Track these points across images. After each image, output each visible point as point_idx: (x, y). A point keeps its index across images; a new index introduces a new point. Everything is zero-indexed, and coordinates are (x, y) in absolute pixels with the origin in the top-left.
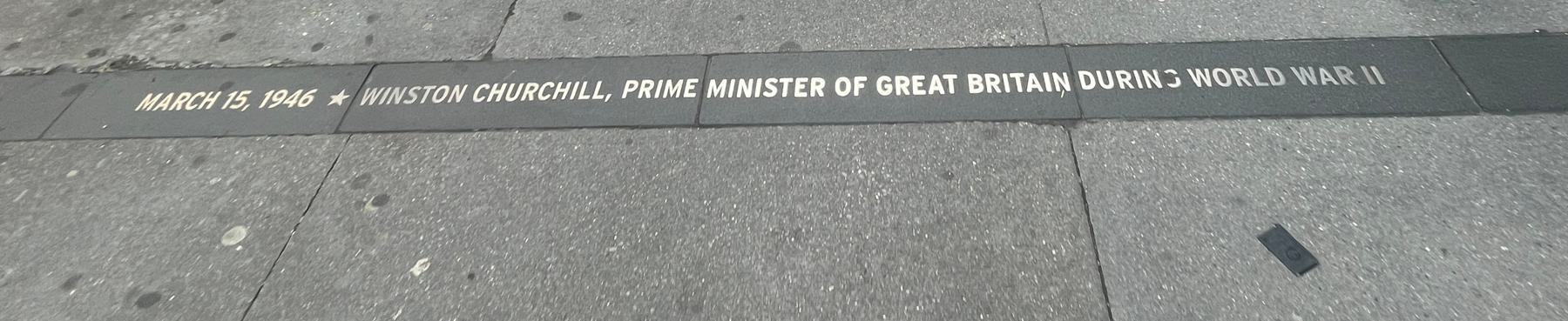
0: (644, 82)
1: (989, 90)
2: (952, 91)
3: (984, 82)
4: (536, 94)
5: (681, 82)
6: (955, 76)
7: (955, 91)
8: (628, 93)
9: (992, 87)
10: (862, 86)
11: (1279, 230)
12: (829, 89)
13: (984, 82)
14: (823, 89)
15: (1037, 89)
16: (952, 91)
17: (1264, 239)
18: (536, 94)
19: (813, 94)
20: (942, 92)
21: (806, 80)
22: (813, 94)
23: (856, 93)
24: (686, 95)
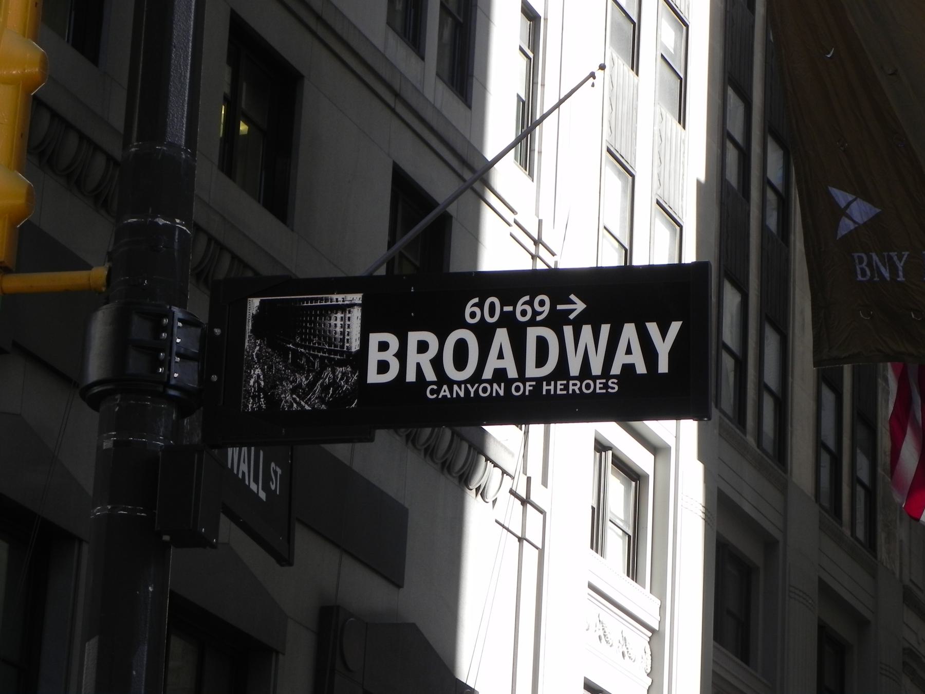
0: (414, 337)
1: (411, 377)
2: (663, 367)
3: (402, 355)
4: (437, 363)
5: (476, 385)
6: (846, 226)
7: (437, 386)
8: (443, 396)
9: (418, 365)
10: (531, 388)
11: (553, 256)
12: (262, 398)
13: (402, 355)
14: (546, 390)
15: (446, 396)
16: (663, 367)
17: (556, 255)
18: (580, 389)
19: (571, 392)
20: (449, 396)
21: (565, 382)
22: (571, 392)
23: (527, 393)
24: (559, 392)
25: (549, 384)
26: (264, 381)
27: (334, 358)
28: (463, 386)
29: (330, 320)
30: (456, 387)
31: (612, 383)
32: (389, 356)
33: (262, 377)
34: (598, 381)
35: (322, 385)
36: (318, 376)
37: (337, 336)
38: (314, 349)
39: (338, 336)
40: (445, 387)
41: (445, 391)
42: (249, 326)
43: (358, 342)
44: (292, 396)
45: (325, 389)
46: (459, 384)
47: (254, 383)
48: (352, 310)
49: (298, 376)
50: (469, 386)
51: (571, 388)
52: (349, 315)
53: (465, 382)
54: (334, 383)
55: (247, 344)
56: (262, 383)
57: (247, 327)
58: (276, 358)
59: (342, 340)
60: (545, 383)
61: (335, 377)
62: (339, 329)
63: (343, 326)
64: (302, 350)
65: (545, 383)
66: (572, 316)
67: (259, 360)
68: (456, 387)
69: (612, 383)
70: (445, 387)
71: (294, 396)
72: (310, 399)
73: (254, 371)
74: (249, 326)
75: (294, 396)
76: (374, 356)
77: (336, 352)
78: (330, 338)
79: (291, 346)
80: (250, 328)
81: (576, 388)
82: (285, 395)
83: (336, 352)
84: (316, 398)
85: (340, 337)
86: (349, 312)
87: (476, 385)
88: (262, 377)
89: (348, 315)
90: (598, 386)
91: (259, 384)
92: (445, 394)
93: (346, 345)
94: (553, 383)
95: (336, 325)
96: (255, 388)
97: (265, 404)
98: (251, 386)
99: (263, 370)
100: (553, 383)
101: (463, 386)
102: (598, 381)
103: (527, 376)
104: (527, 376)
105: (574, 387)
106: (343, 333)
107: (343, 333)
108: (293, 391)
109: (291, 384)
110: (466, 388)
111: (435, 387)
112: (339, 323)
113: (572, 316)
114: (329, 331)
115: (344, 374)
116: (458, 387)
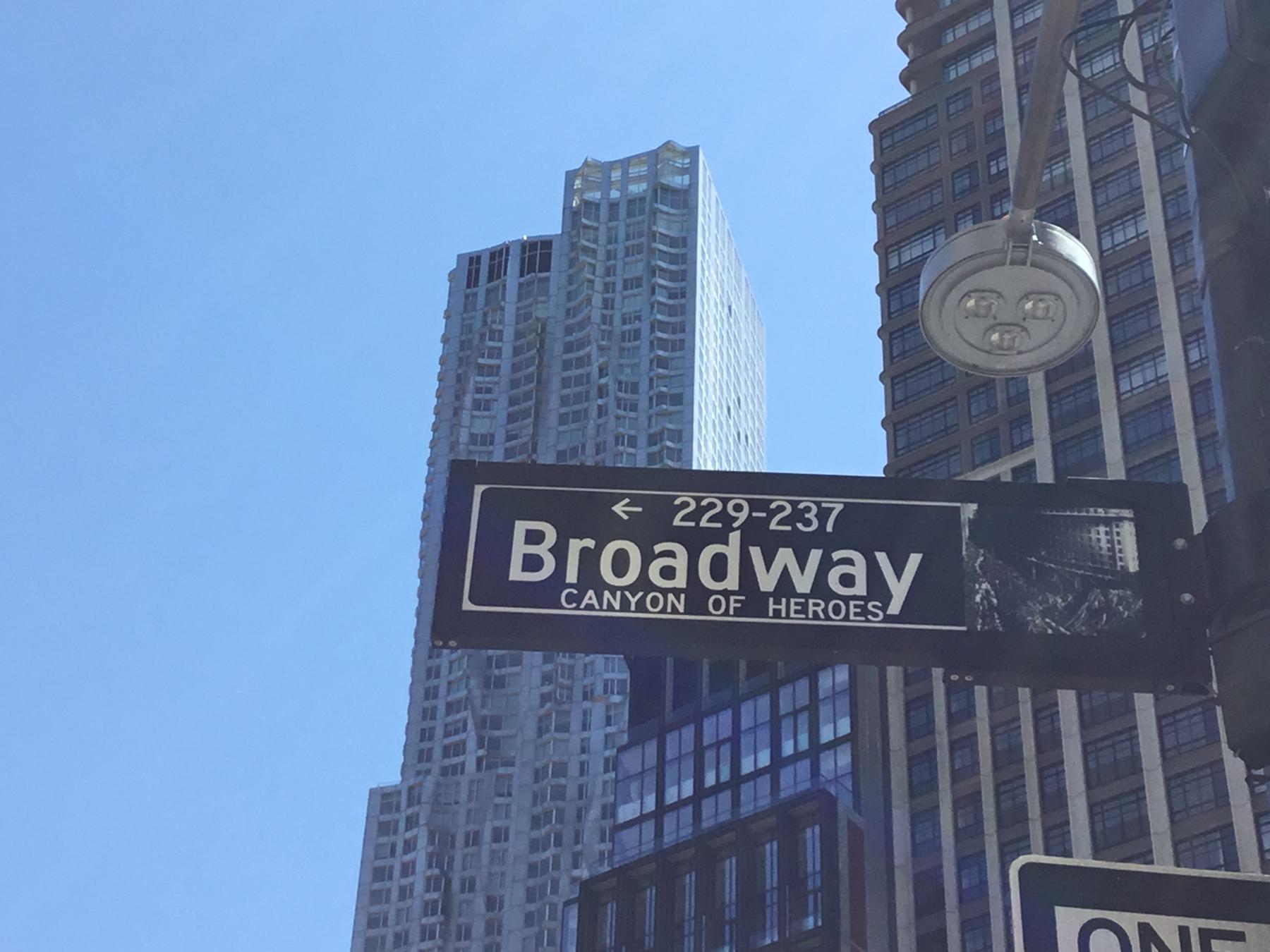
5: (640, 594)
25: (777, 602)
26: (996, 598)
27: (1103, 579)
28: (619, 593)
29: (1090, 533)
30: (607, 594)
31: (874, 606)
32: (542, 550)
33: (992, 593)
34: (732, 598)
35: (1088, 609)
36: (1082, 597)
37: (1103, 552)
38: (1072, 566)
39: (1104, 552)
40: (591, 593)
41: (590, 598)
42: (966, 532)
43: (1137, 562)
44: (1043, 619)
45: (1094, 614)
46: (613, 590)
47: (982, 599)
48: (1121, 524)
49: (1049, 596)
50: (627, 593)
51: (811, 609)
52: (1118, 530)
53: (622, 589)
54: (1107, 607)
55: (964, 553)
56: (995, 601)
57: (963, 534)
58: (1011, 572)
59: (1113, 558)
60: (771, 600)
61: (1108, 601)
62: (1104, 545)
63: (1110, 541)
64: (1052, 565)
65: (771, 600)
66: (627, 500)
67: (984, 574)
68: (607, 594)
69: (874, 606)
70: (591, 593)
71: (1047, 620)
72: (1073, 625)
73: (980, 585)
74: (966, 532)
75: (1047, 620)
76: (520, 549)
77: (1106, 572)
78: (1092, 555)
79: (1033, 559)
80: (967, 533)
81: (819, 609)
82: (1033, 617)
83: (1106, 572)
84: (1082, 625)
85: (1108, 553)
86: (1117, 526)
87: (640, 594)
88: (992, 593)
89: (1115, 530)
90: (852, 610)
91: (990, 602)
92: (590, 602)
93: (1119, 563)
94: (784, 600)
95: (1099, 540)
96: (984, 607)
97: (1002, 626)
98: (977, 603)
99: (993, 585)
100: (784, 600)
101: (619, 593)
102: (732, 598)
103: (567, 581)
104: (567, 581)
105: (816, 608)
106: (1111, 549)
107: (1111, 549)
108: (1044, 614)
109: (1041, 605)
110: (623, 597)
111: (575, 592)
112: (1103, 537)
113: (627, 500)
114: (1090, 546)
115: (1121, 599)
116: (611, 594)
